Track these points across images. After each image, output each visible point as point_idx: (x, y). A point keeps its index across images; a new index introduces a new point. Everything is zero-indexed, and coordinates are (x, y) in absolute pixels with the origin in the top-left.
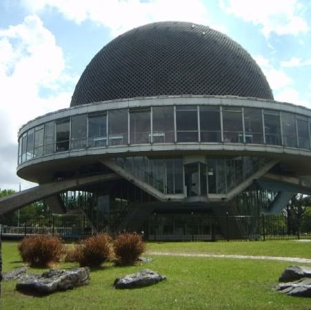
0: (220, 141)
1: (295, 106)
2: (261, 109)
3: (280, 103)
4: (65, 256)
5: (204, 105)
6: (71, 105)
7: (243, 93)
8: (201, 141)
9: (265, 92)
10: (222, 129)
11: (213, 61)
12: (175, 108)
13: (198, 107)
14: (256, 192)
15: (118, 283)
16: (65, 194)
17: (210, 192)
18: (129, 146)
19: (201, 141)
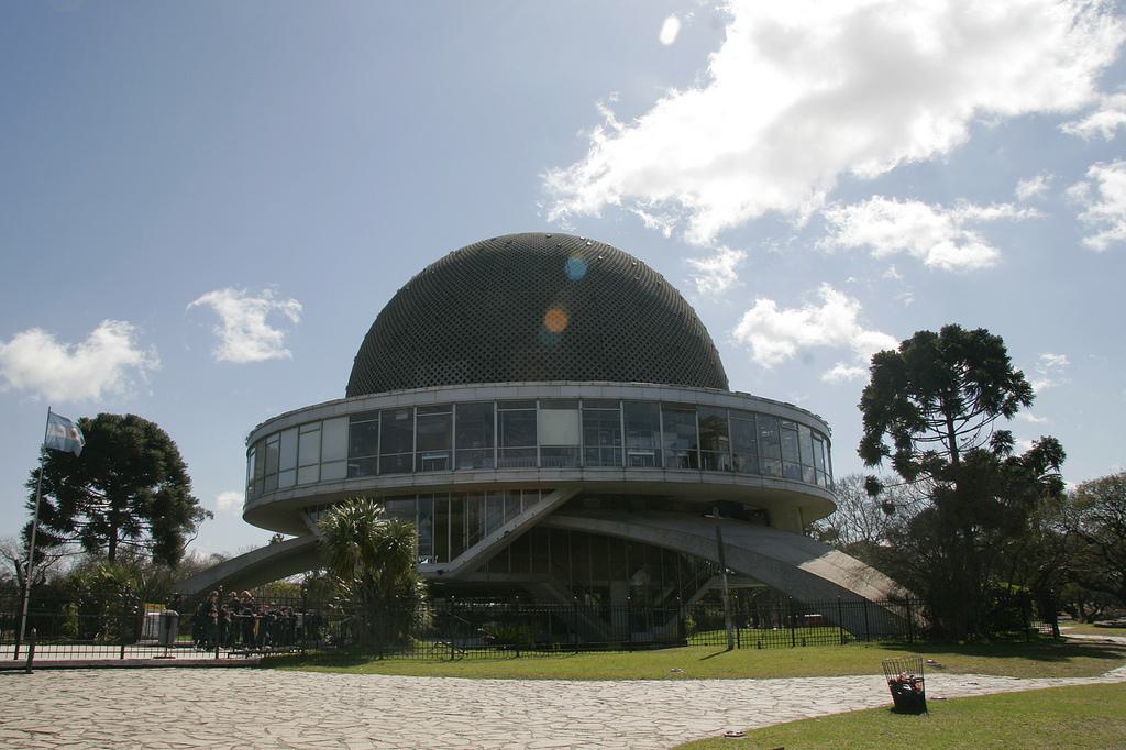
7: (673, 379)
9: (716, 379)
19: (382, 473)
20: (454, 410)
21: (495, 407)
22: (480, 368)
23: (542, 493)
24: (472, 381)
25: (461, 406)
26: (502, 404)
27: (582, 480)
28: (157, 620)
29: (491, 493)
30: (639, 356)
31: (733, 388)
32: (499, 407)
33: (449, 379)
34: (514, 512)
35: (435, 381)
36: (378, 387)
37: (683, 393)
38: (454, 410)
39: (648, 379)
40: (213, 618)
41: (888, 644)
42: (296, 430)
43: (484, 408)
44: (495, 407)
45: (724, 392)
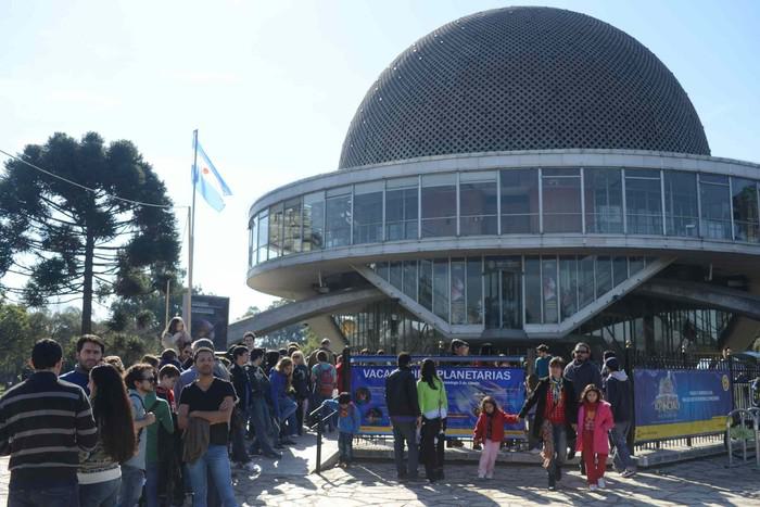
0: (497, 234)
1: (739, 163)
2: (694, 173)
3: (720, 160)
4: (684, 400)
5: (673, 171)
6: (341, 167)
7: (650, 142)
8: (423, 236)
9: (698, 144)
10: (499, 211)
11: (646, 74)
12: (623, 171)
13: (662, 173)
14: (691, 315)
15: (351, 477)
16: (691, 315)
17: (527, 322)
18: (383, 243)
19: (423, 236)
20: (582, 173)
21: (623, 175)
22: (474, 138)
23: (526, 259)
24: (532, 147)
25: (589, 170)
26: (630, 171)
27: (323, 261)
28: (83, 414)
29: (581, 257)
30: (463, 115)
31: (714, 154)
32: (626, 175)
33: (444, 149)
34: (621, 276)
35: (423, 152)
36: (383, 156)
37: (607, 156)
38: (582, 173)
39: (604, 144)
40: (90, 416)
41: (720, 477)
42: (323, 193)
43: (612, 172)
44: (623, 175)
45: (705, 157)
